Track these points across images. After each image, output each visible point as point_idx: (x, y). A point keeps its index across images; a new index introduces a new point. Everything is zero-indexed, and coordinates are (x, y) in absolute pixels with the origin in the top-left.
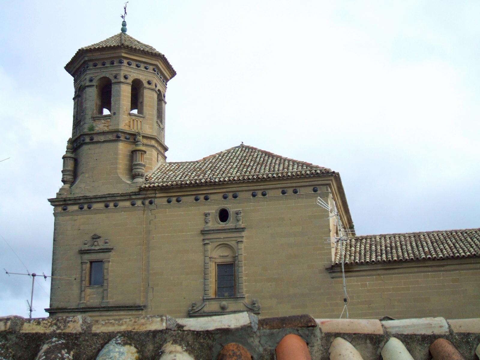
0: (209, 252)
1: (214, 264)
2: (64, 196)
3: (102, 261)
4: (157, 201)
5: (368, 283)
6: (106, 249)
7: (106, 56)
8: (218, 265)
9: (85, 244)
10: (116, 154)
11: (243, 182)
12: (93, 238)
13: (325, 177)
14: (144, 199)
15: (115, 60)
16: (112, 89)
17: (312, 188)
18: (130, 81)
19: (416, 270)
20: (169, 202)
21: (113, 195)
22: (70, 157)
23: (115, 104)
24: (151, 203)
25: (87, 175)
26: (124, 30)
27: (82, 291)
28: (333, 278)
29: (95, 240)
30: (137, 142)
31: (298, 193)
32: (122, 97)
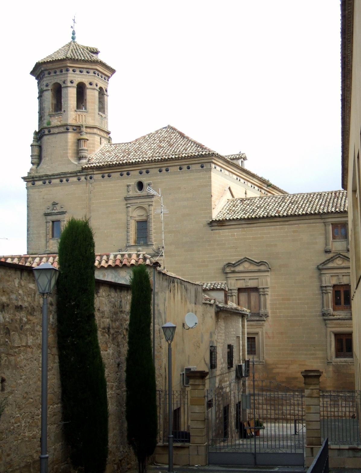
0: (130, 213)
1: (134, 221)
2: (32, 175)
3: (59, 221)
4: (95, 177)
5: (235, 234)
6: (62, 212)
7: (57, 66)
8: (137, 222)
9: (48, 209)
10: (67, 142)
11: (158, 161)
12: (53, 205)
13: (208, 157)
14: (86, 175)
15: (63, 69)
16: (62, 93)
17: (200, 165)
18: (75, 84)
19: (269, 224)
20: (103, 177)
21: (65, 173)
22: (35, 145)
23: (65, 104)
24: (91, 178)
25: (47, 159)
26: (73, 38)
27: (47, 242)
28: (212, 230)
29: (54, 206)
30: (81, 132)
31: (191, 169)
32: (69, 98)
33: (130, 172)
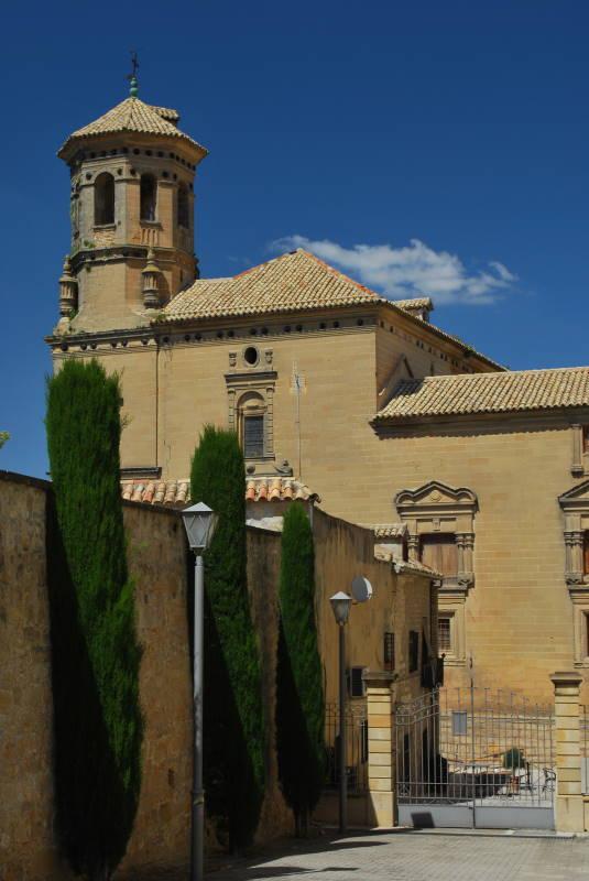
33: (235, 331)
